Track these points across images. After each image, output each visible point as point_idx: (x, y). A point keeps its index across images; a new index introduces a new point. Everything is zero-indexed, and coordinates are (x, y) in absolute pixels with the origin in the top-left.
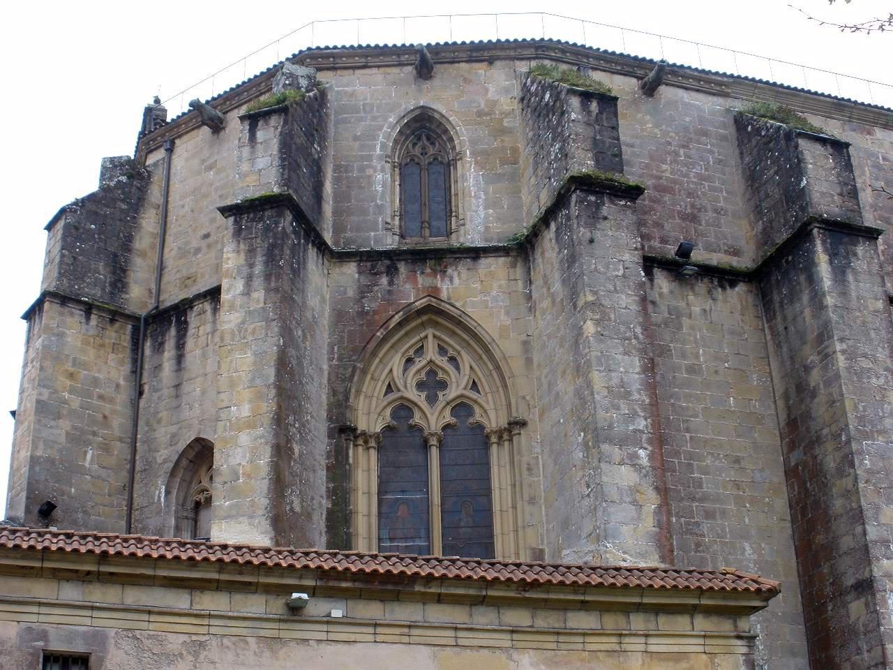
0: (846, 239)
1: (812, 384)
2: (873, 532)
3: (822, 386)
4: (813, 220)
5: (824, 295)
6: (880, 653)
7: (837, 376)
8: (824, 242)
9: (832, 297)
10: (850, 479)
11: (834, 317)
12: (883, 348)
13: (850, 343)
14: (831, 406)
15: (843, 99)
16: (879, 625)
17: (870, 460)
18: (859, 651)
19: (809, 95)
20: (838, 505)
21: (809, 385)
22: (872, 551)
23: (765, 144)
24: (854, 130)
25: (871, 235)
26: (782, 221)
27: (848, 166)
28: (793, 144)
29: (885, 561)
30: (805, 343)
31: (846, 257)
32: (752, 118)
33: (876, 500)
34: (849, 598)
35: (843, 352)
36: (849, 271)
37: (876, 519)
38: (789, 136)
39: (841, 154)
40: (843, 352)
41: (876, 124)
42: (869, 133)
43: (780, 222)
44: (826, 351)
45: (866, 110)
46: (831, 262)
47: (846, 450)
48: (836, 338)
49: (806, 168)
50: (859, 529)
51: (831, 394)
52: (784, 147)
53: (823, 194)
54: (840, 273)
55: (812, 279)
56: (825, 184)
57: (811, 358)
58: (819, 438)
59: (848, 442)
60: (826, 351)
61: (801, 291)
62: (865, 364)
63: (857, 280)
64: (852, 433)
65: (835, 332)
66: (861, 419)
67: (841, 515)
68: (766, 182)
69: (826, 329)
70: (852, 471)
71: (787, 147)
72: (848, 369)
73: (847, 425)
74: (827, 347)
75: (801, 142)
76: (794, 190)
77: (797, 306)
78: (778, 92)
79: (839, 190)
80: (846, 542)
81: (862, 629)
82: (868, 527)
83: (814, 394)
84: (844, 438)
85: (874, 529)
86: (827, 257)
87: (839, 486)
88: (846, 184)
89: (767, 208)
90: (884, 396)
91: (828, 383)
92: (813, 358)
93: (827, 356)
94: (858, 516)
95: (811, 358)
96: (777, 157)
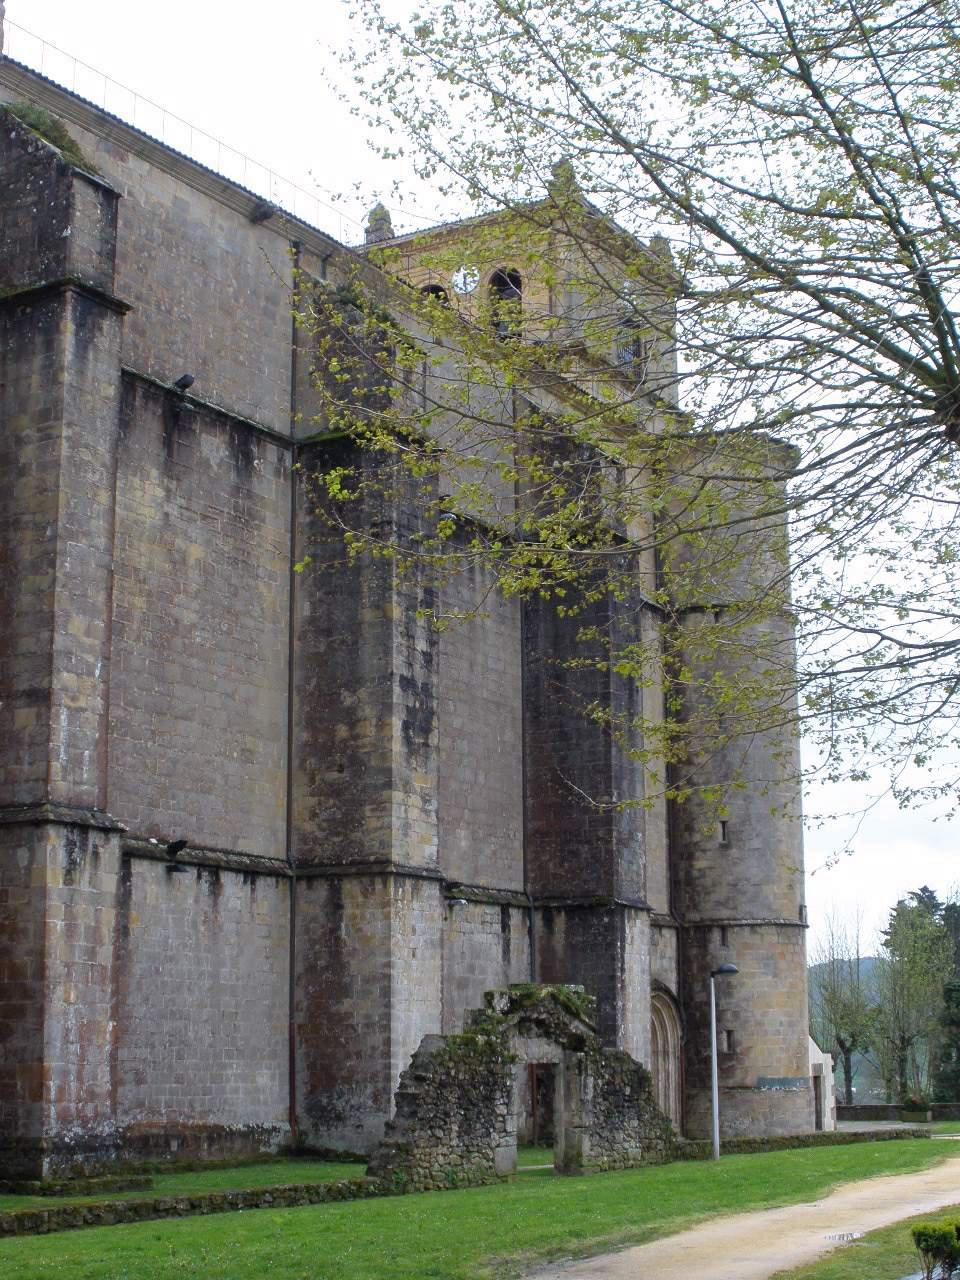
0: (95, 310)
1: (22, 460)
2: (60, 642)
3: (34, 467)
4: (70, 282)
5: (62, 369)
6: (44, 769)
7: (57, 464)
8: (74, 309)
9: (70, 374)
10: (47, 581)
11: (67, 397)
12: (105, 441)
13: (77, 429)
14: (41, 493)
15: (109, 114)
16: (48, 740)
17: (71, 563)
18: (18, 760)
19: (76, 101)
20: (25, 601)
21: (18, 461)
22: (55, 661)
23: (30, 164)
24: (108, 152)
25: (120, 309)
26: (28, 262)
27: (113, 222)
28: (66, 181)
29: (65, 674)
30: (24, 412)
31: (92, 331)
32: (19, 124)
33: (68, 607)
34: (19, 703)
35: (69, 439)
36: (91, 347)
37: (65, 627)
38: (63, 170)
39: (110, 205)
40: (69, 439)
41: (130, 148)
42: (122, 160)
43: (24, 262)
44: (49, 431)
45: (128, 133)
46: (77, 334)
47: (50, 547)
48: (64, 421)
49: (74, 215)
50: (45, 635)
51: (43, 480)
52: (53, 180)
53: (83, 249)
54: (83, 346)
55: (51, 345)
56: (87, 238)
57: (28, 431)
58: (17, 522)
59: (54, 538)
60: (49, 431)
61: (34, 353)
62: (87, 456)
63: (96, 359)
64: (60, 531)
65: (65, 414)
66: (71, 517)
67: (27, 614)
68: (19, 208)
69: (55, 407)
70: (50, 571)
71: (58, 181)
72: (70, 458)
73: (56, 521)
74: (51, 427)
75: (77, 183)
76: (53, 235)
77: (24, 369)
78: (45, 88)
79: (98, 250)
80: (27, 644)
81: (27, 739)
82: (56, 635)
83: (22, 472)
84: (48, 533)
85: (61, 638)
86: (74, 327)
87: (29, 582)
88: (107, 242)
89: (10, 238)
90: (95, 495)
91: (43, 467)
92: (30, 432)
93: (49, 437)
94: (48, 621)
95: (28, 431)
96: (41, 186)
